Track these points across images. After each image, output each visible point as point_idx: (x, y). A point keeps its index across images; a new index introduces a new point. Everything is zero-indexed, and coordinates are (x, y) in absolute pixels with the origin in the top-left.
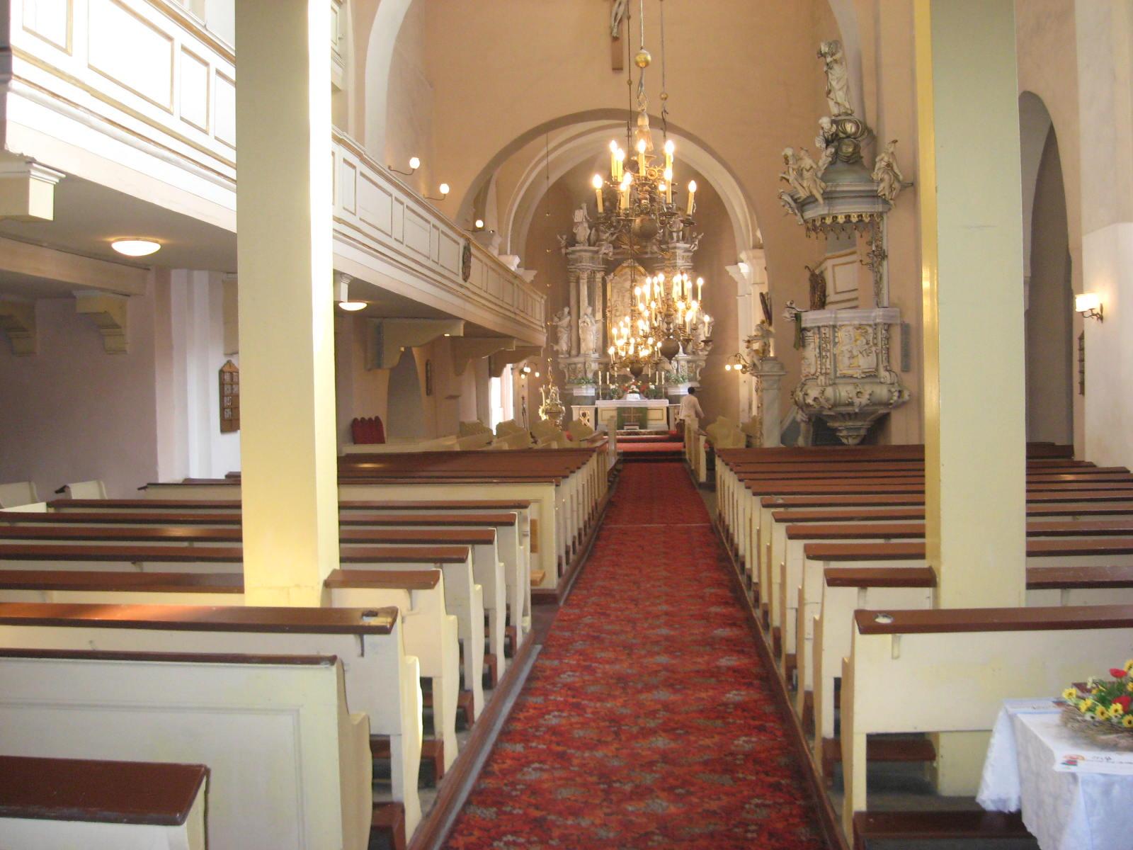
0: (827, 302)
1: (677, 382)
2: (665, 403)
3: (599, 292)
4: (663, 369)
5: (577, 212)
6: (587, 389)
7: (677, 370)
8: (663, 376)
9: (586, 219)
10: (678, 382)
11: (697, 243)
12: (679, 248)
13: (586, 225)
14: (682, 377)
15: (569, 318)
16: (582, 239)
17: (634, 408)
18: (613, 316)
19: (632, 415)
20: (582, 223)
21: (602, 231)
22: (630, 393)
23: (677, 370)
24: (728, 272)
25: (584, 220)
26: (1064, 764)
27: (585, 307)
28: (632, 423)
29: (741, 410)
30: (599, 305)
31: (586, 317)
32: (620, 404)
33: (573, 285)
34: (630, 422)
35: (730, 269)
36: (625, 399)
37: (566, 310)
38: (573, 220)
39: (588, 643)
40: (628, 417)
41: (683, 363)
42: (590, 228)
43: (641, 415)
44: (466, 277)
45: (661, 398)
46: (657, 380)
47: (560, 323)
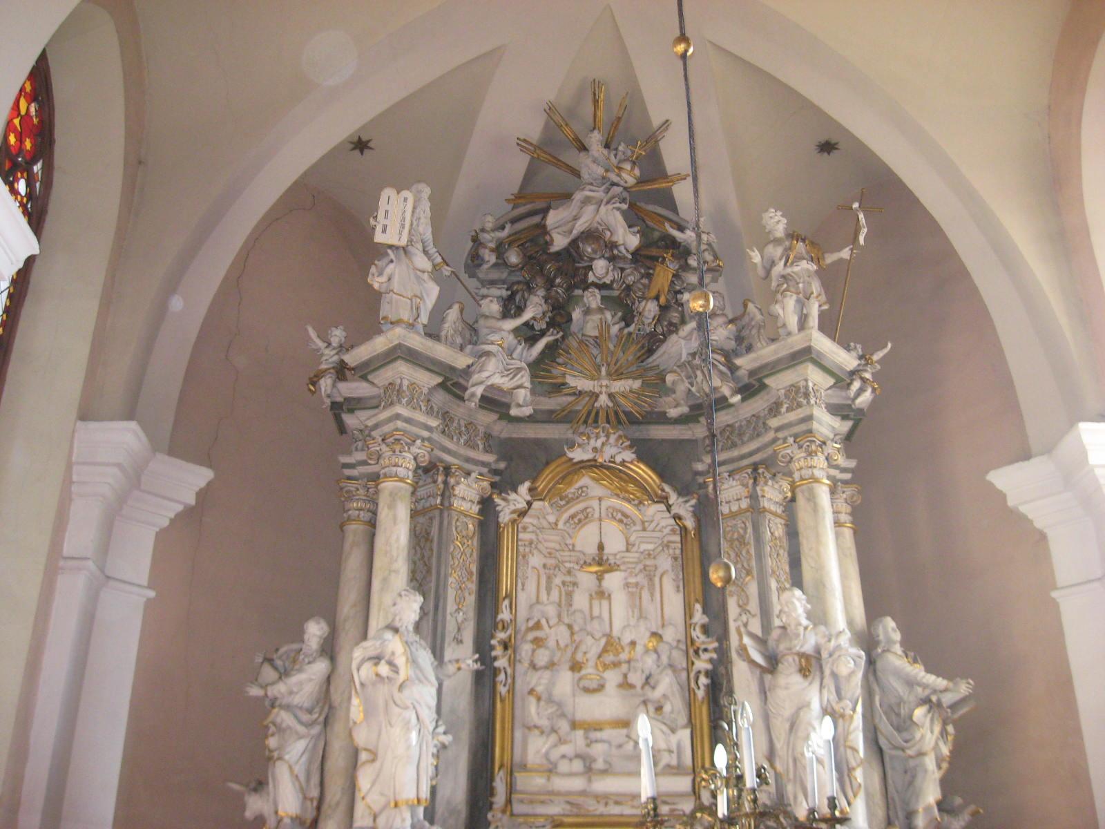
15: (320, 667)
16: (406, 315)
18: (521, 668)
24: (1002, 496)
30: (460, 612)
31: (389, 635)
33: (355, 530)
37: (315, 631)
39: (656, 235)
47: (280, 689)
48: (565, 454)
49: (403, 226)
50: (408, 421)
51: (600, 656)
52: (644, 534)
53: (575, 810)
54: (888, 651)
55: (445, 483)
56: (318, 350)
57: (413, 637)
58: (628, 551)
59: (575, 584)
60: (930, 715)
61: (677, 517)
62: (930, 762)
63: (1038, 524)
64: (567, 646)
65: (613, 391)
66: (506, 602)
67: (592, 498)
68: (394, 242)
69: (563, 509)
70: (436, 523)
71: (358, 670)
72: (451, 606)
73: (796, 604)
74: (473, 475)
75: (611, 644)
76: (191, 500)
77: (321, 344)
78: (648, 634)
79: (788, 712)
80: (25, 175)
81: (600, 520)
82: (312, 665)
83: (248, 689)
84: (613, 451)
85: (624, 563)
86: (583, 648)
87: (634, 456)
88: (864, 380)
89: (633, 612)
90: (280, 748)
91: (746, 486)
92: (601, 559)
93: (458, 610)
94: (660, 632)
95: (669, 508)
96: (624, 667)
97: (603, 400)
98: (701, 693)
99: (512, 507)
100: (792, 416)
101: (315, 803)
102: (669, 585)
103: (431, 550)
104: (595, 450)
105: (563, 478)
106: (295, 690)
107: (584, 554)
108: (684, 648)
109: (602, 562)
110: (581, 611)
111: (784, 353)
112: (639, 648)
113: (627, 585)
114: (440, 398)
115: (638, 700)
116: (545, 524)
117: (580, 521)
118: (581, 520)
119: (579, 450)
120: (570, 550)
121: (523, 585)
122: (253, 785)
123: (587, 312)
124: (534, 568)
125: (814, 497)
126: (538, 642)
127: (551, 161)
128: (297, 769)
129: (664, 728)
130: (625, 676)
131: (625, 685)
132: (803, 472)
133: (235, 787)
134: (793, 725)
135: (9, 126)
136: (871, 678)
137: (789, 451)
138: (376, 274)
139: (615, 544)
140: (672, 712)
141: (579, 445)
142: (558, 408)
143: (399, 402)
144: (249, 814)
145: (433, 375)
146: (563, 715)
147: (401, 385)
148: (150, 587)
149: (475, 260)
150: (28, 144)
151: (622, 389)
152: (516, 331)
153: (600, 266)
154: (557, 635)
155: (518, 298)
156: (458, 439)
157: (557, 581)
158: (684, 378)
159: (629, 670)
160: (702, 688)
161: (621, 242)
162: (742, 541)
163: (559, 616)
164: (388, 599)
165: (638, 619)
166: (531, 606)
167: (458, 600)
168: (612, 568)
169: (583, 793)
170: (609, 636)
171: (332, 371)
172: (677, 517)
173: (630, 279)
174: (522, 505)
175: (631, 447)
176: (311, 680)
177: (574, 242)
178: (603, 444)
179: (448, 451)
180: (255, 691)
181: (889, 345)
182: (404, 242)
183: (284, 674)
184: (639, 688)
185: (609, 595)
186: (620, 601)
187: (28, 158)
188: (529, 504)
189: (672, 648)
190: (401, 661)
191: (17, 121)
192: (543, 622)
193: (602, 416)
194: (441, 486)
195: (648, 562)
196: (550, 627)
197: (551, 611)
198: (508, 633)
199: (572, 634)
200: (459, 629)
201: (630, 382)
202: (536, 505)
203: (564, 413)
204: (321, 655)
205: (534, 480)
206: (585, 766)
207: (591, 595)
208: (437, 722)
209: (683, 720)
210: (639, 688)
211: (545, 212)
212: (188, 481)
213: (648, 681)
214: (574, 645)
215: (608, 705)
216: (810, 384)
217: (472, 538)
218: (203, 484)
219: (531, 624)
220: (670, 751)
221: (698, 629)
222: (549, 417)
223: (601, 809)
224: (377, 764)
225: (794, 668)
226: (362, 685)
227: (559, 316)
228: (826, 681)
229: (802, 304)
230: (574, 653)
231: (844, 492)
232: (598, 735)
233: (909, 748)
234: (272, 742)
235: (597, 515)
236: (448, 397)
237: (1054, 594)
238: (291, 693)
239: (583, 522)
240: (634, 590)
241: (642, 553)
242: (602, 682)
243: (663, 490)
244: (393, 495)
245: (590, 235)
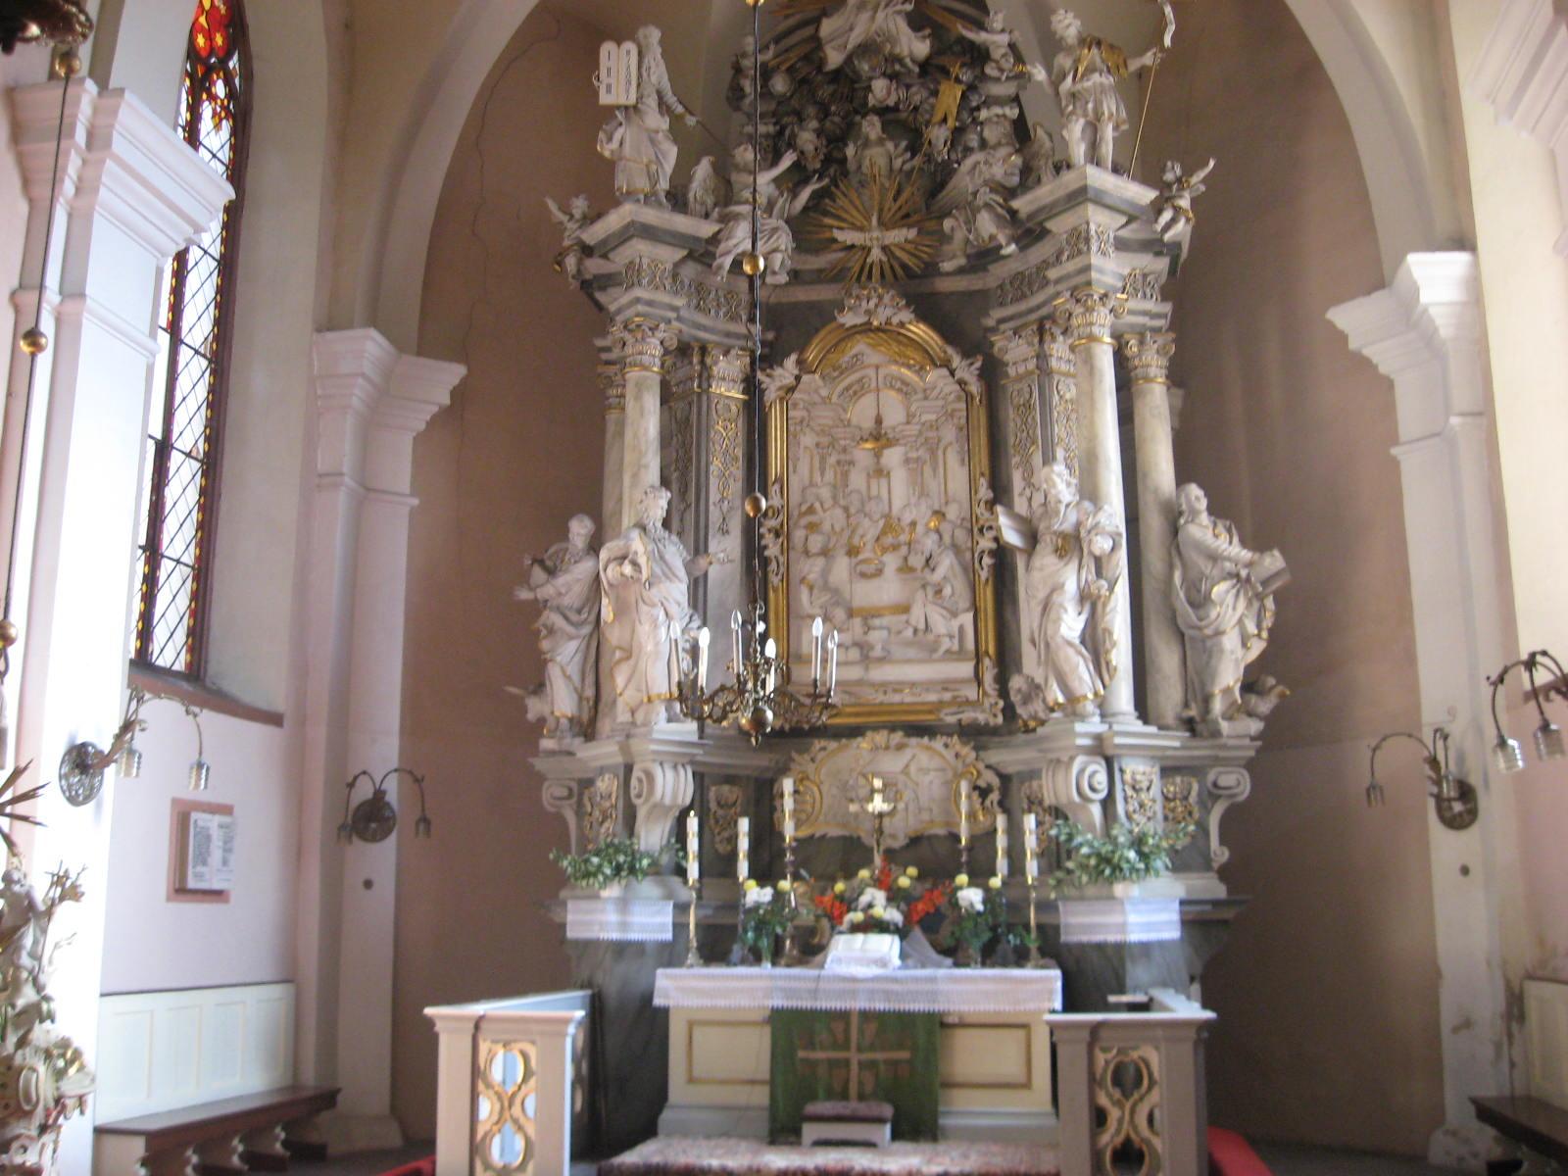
1: (1107, 868)
2: (1039, 988)
3: (725, 437)
4: (1034, 803)
6: (624, 904)
7: (1108, 803)
8: (1031, 842)
10: (1117, 868)
11: (1184, 203)
12: (1100, 200)
14: (1138, 843)
16: (642, 184)
17: (866, 1016)
19: (854, 1057)
20: (633, 110)
22: (856, 928)
23: (1108, 803)
24: (1342, 338)
25: (652, 102)
26: (1474, 1101)
27: (641, 490)
28: (853, 1106)
29: (1448, 1018)
31: (635, 534)
32: (789, 993)
34: (844, 1096)
35: (1355, 320)
36: (822, 966)
38: (595, 94)
40: (832, 1064)
41: (1137, 769)
43: (904, 1055)
44: (217, 895)
45: (1020, 958)
46: (1002, 864)
48: (835, 319)
50: (650, 303)
51: (878, 539)
52: (926, 403)
53: (853, 700)
54: (1192, 521)
55: (702, 362)
56: (561, 223)
57: (661, 532)
58: (908, 423)
59: (851, 463)
60: (1234, 591)
61: (961, 383)
62: (1230, 641)
63: (1383, 369)
64: (843, 530)
65: (887, 242)
66: (777, 487)
67: (869, 366)
68: (622, 101)
69: (837, 381)
70: (695, 409)
71: (605, 570)
72: (714, 496)
73: (1061, 483)
74: (733, 352)
75: (890, 525)
76: (446, 400)
77: (564, 218)
78: (930, 513)
79: (1041, 595)
80: (221, 74)
81: (878, 390)
82: (579, 565)
83: (517, 593)
84: (889, 312)
85: (904, 437)
86: (860, 531)
87: (912, 316)
88: (1177, 210)
89: (914, 490)
90: (552, 650)
91: (1030, 344)
92: (879, 433)
93: (722, 500)
94: (943, 509)
95: (952, 373)
96: (904, 550)
97: (876, 254)
98: (984, 574)
99: (778, 384)
100: (1070, 267)
101: (591, 703)
102: (953, 459)
103: (692, 437)
104: (868, 312)
105: (836, 345)
106: (563, 591)
107: (860, 429)
108: (969, 526)
109: (879, 437)
110: (859, 492)
111: (1061, 193)
112: (920, 529)
113: (907, 461)
114: (690, 271)
115: (918, 584)
116: (816, 399)
117: (855, 393)
118: (856, 392)
119: (850, 314)
120: (845, 426)
121: (795, 467)
122: (531, 688)
123: (867, 144)
124: (806, 448)
125: (1091, 358)
126: (812, 527)
128: (569, 670)
129: (945, 613)
130: (906, 559)
131: (905, 568)
132: (1081, 329)
133: (513, 690)
134: (1046, 606)
135: (195, 29)
136: (1174, 552)
137: (1068, 306)
138: (605, 140)
139: (894, 412)
140: (953, 594)
141: (850, 309)
142: (828, 266)
143: (640, 284)
144: (531, 716)
145: (676, 249)
146: (837, 604)
147: (640, 265)
148: (412, 495)
149: (736, 94)
150: (219, 40)
151: (897, 240)
152: (776, 181)
153: (880, 86)
154: (832, 518)
155: (787, 132)
156: (717, 313)
157: (832, 460)
158: (963, 225)
159: (909, 552)
160: (986, 569)
161: (906, 52)
162: (1028, 406)
163: (834, 498)
164: (638, 495)
165: (919, 498)
166: (804, 490)
167: (721, 488)
168: (891, 443)
169: (860, 682)
170: (887, 516)
171: (576, 248)
172: (961, 383)
173: (917, 99)
174: (790, 380)
175: (908, 305)
176: (578, 580)
177: (849, 60)
178: (876, 306)
179: (705, 329)
180: (524, 595)
181: (1212, 163)
182: (632, 100)
183: (551, 572)
184: (919, 571)
185: (889, 473)
186: (899, 478)
187: (221, 55)
188: (798, 378)
189: (955, 526)
190: (642, 560)
191: (202, 20)
192: (817, 505)
193: (876, 272)
194: (697, 367)
195: (931, 434)
196: (824, 511)
197: (825, 493)
198: (779, 520)
199: (848, 517)
200: (724, 519)
201: (904, 231)
202: (805, 378)
203: (835, 271)
204: (588, 554)
205: (802, 350)
206: (861, 655)
207: (868, 474)
208: (691, 617)
209: (964, 602)
210: (919, 571)
211: (816, 21)
212: (443, 379)
213: (929, 563)
214: (851, 529)
215: (887, 589)
216: (1093, 227)
217: (736, 421)
218: (456, 381)
219: (804, 508)
220: (951, 637)
221: (982, 504)
222: (820, 277)
223: (880, 698)
224: (632, 662)
225: (1050, 548)
226: (611, 585)
227: (835, 140)
228: (1085, 560)
229: (1093, 129)
230: (850, 537)
231: (1155, 342)
232: (877, 622)
233: (1207, 627)
234: (545, 645)
235: (873, 385)
236: (699, 267)
237: (1394, 451)
238: (560, 594)
239: (859, 394)
240: (915, 466)
241: (924, 424)
242: (880, 567)
243: (945, 352)
244: (640, 387)
245: (866, 49)
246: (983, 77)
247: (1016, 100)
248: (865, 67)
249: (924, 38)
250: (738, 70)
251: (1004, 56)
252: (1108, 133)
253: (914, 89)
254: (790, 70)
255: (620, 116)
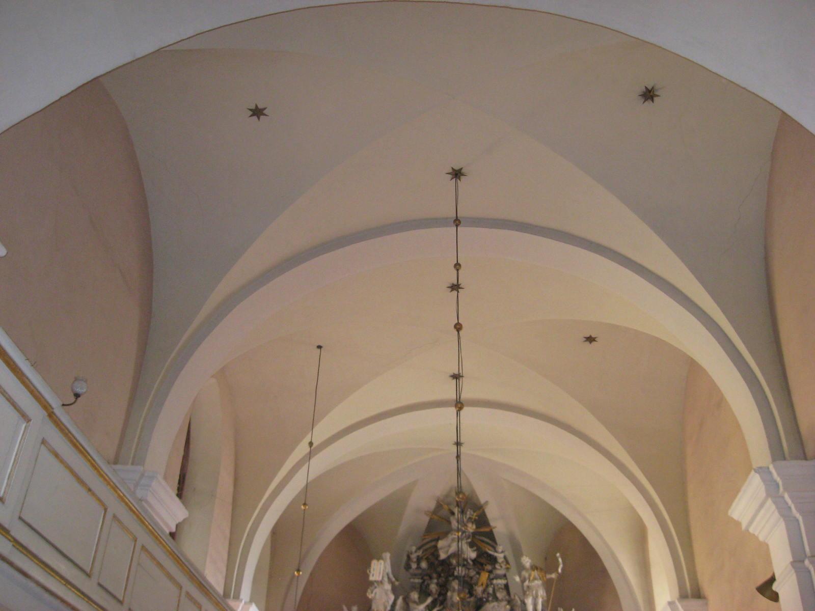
0: (769, 502)
5: (374, 563)
9: (389, 578)
13: (388, 587)
20: (381, 582)
21: (415, 602)
25: (386, 579)
38: (368, 576)
42: (394, 590)
49: (380, 573)
127: (438, 524)
149: (408, 567)
155: (426, 583)
177: (449, 557)
182: (380, 579)
211: (437, 540)
227: (444, 588)
246: (495, 568)
247: (505, 576)
248: (454, 562)
249: (474, 551)
250: (409, 557)
251: (503, 562)
252: (540, 601)
253: (471, 571)
254: (427, 559)
255: (376, 584)
